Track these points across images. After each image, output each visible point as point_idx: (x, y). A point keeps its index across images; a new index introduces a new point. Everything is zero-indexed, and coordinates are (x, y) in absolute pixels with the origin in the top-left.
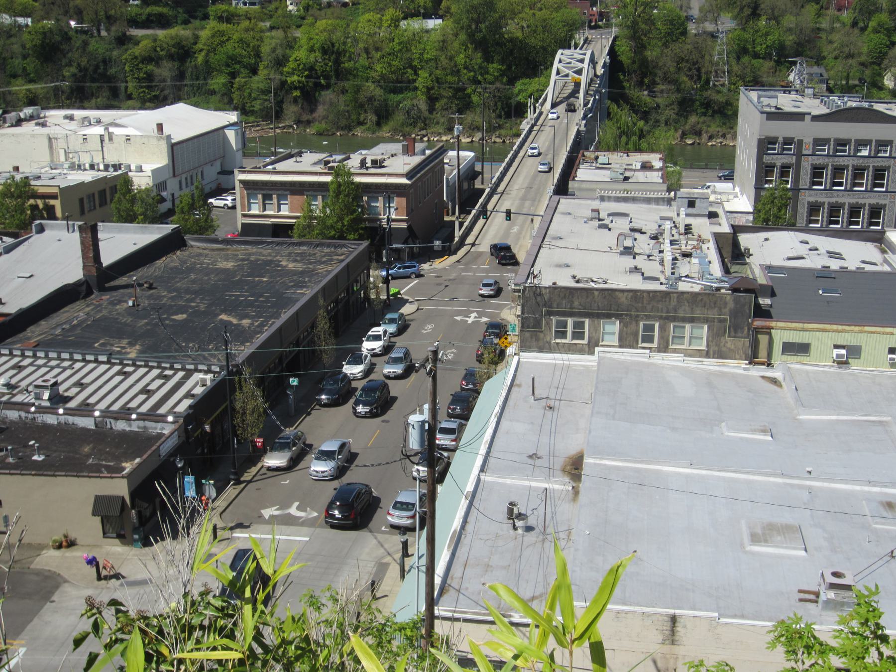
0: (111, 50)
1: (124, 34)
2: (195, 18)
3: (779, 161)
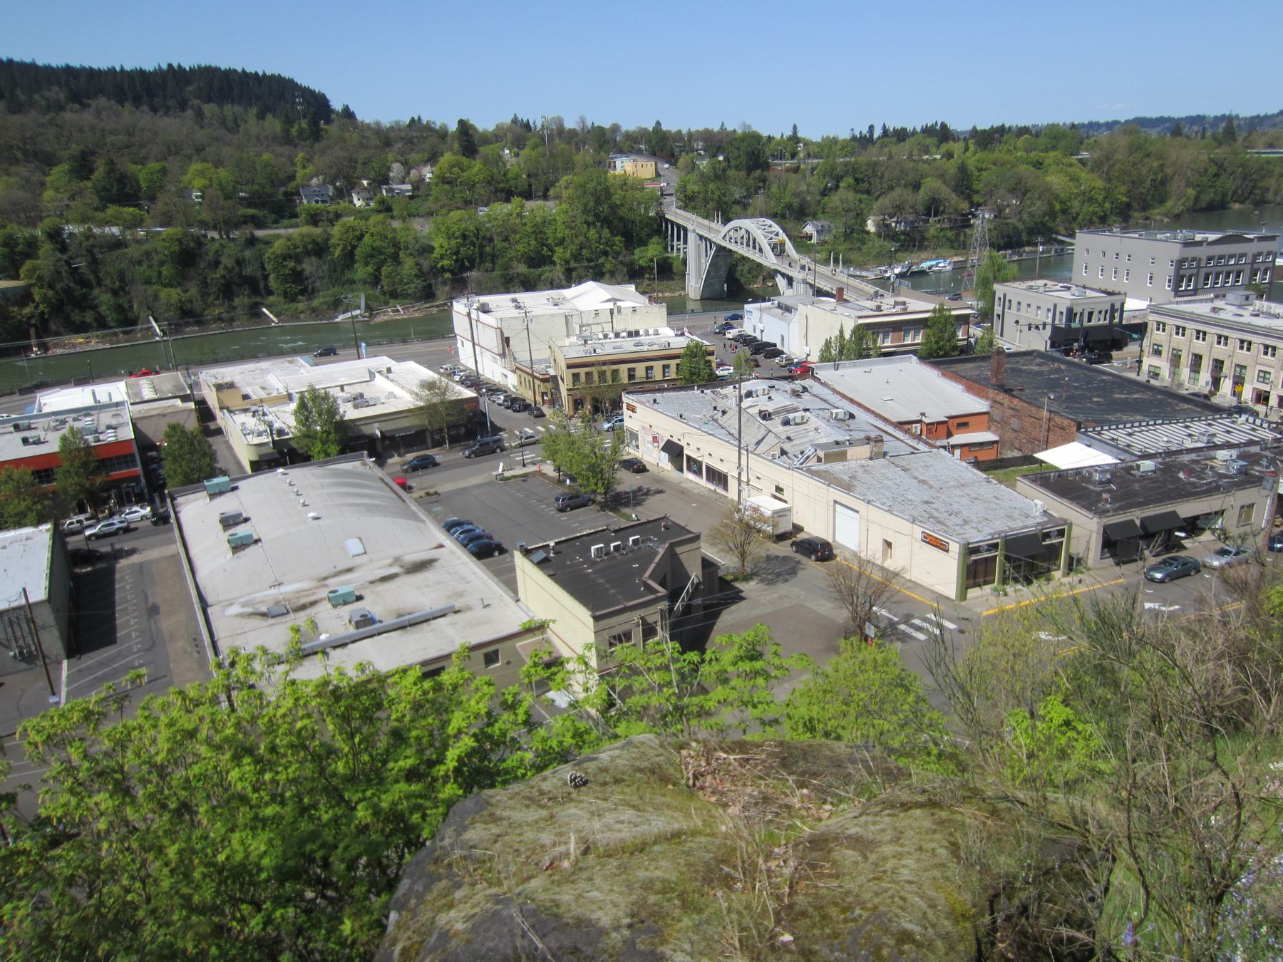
0: (242, 251)
1: (253, 236)
2: (283, 217)
3: (1188, 273)
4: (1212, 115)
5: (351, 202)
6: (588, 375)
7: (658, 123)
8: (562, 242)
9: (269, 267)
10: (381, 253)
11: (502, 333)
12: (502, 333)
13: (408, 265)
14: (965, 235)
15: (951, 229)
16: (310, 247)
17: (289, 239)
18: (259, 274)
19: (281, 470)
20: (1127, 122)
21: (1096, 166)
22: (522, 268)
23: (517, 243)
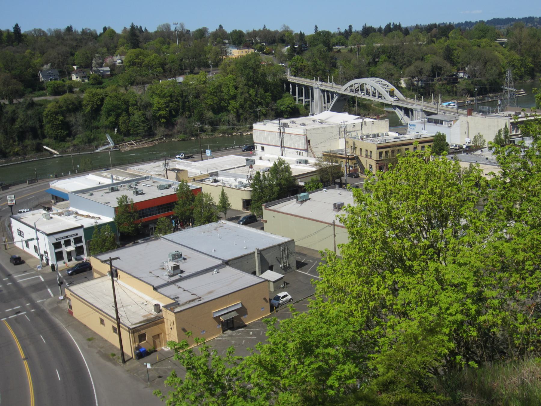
2: (35, 90)
4: (538, 17)
5: (71, 79)
6: (387, 152)
7: (265, 27)
8: (234, 97)
9: (45, 120)
10: (119, 108)
11: (307, 138)
12: (307, 138)
13: (137, 116)
14: (456, 87)
15: (448, 84)
16: (70, 107)
17: (57, 102)
18: (37, 125)
19: (325, 190)
20: (488, 21)
21: (513, 47)
22: (209, 114)
23: (205, 99)
